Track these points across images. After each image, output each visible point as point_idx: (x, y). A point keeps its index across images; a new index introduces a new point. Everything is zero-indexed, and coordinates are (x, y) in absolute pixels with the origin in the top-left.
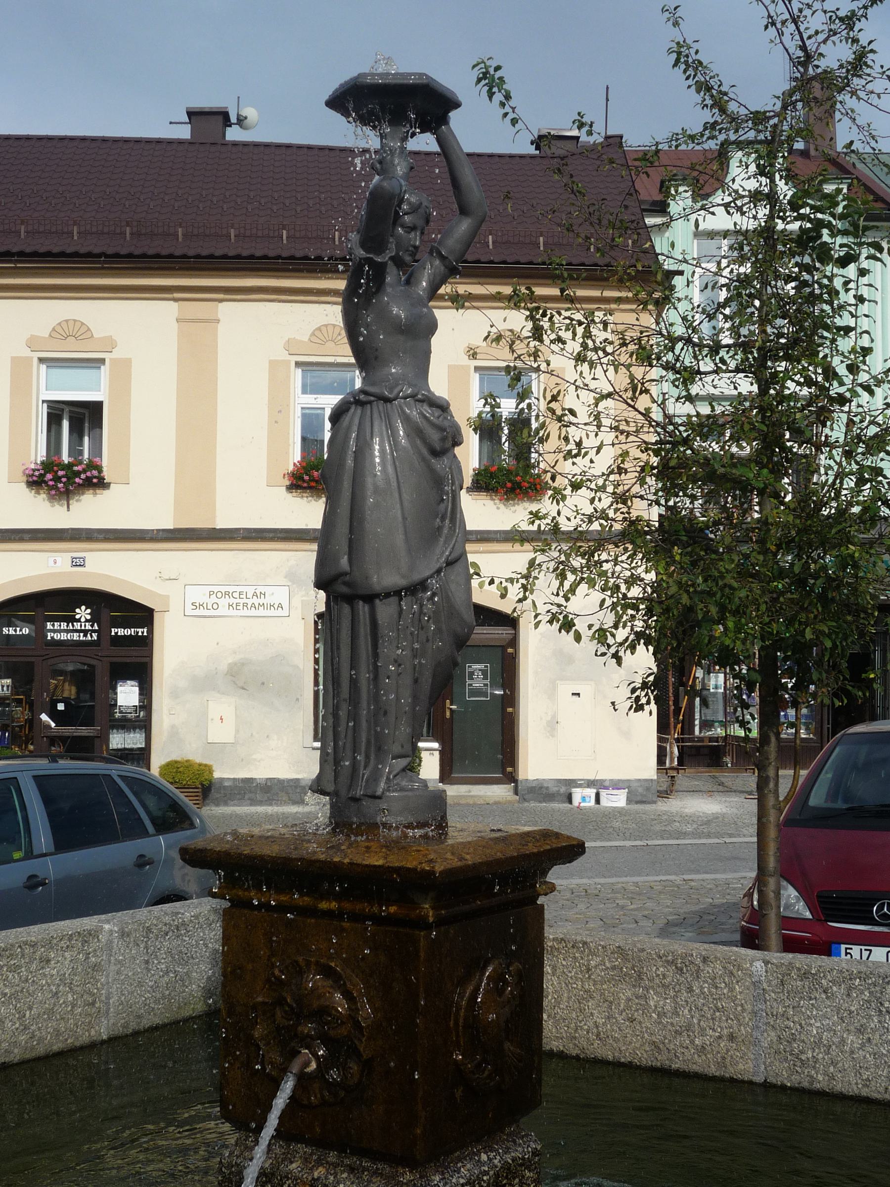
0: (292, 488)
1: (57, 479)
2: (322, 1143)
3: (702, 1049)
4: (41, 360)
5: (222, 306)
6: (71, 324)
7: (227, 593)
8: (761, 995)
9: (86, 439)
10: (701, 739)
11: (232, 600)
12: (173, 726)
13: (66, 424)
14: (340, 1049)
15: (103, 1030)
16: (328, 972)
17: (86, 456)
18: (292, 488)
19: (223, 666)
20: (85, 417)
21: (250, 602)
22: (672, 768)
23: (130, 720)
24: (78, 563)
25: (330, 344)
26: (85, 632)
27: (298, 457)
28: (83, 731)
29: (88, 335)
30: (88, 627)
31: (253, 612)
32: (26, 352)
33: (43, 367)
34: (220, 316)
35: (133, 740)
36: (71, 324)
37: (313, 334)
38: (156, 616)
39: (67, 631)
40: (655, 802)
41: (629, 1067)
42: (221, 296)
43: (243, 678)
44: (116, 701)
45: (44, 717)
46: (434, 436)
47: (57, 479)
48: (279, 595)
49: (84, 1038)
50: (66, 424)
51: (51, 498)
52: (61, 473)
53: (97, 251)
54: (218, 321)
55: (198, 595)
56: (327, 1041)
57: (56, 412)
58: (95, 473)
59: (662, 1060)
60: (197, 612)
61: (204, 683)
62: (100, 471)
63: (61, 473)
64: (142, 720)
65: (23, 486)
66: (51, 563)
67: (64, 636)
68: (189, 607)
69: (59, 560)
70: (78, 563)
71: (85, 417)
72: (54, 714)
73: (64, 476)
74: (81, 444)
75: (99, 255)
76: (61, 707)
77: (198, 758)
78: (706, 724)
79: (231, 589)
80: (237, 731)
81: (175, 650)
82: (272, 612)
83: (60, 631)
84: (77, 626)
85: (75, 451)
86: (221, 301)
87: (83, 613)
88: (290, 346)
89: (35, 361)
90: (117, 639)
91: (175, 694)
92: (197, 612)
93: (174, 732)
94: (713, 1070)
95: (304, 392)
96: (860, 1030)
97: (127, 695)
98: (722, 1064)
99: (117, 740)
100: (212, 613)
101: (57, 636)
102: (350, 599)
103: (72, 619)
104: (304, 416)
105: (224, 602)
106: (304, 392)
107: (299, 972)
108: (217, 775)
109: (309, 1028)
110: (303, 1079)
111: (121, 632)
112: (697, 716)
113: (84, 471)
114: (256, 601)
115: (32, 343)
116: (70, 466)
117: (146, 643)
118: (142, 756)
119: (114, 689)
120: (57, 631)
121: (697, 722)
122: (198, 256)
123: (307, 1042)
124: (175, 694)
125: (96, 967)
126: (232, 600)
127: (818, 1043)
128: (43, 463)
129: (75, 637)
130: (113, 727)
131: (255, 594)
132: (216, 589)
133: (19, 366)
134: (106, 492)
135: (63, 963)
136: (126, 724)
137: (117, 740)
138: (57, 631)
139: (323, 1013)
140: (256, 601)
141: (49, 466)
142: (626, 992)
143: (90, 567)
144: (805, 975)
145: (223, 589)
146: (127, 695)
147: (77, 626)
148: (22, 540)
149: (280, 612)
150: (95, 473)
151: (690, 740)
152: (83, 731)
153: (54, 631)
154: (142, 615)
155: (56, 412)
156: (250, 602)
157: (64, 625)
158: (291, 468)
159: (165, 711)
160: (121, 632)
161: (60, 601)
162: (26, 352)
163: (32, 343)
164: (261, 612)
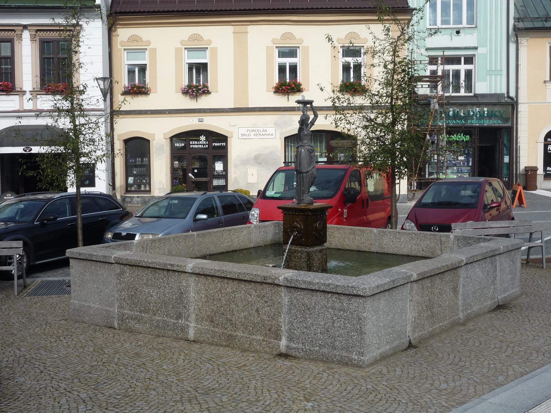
0: (276, 92)
1: (193, 91)
2: (297, 245)
3: (366, 247)
4: (185, 48)
5: (249, 27)
6: (196, 35)
7: (253, 130)
8: (376, 236)
9: (201, 75)
10: (428, 179)
11: (255, 133)
12: (235, 178)
13: (194, 71)
14: (299, 232)
15: (252, 245)
16: (297, 222)
17: (201, 83)
18: (276, 92)
19: (253, 156)
20: (201, 68)
21: (261, 133)
22: (414, 190)
23: (220, 175)
24: (201, 121)
25: (288, 40)
26: (204, 145)
27: (277, 81)
28: (204, 179)
29: (202, 39)
30: (205, 143)
31: (263, 137)
32: (180, 46)
33: (186, 51)
34: (248, 30)
35: (221, 182)
36: (196, 35)
37: (282, 36)
38: (229, 139)
39: (197, 144)
40: (406, 202)
41: (353, 251)
42: (249, 23)
43: (258, 160)
44: (215, 168)
45: (190, 175)
46: (311, 151)
47: (193, 91)
48: (271, 131)
49: (249, 247)
50: (194, 71)
51: (191, 98)
52: (194, 89)
53: (204, 9)
54: (248, 33)
55: (243, 131)
56: (297, 231)
57: (191, 67)
58: (206, 89)
59: (359, 249)
60: (243, 137)
61: (246, 162)
62: (208, 88)
63: (194, 89)
64: (224, 175)
65: (181, 94)
66: (191, 121)
67: (196, 146)
68: (240, 135)
69: (194, 120)
70: (201, 121)
71: (201, 68)
72: (194, 174)
73: (195, 90)
74: (200, 77)
75: (205, 11)
76: (196, 171)
77: (244, 189)
78: (430, 174)
79: (255, 129)
80: (258, 179)
81: (236, 150)
82: (269, 137)
83: (195, 144)
84: (201, 142)
85: (198, 81)
86: (249, 25)
87: (203, 138)
88: (273, 41)
89: (183, 49)
90: (215, 147)
91: (236, 166)
92: (243, 137)
93: (236, 179)
94: (368, 250)
95: (279, 57)
96: (393, 242)
97: (219, 166)
98: (369, 249)
99: (216, 182)
100: (248, 137)
101: (194, 146)
102: (300, 173)
103: (199, 140)
104: (279, 66)
105: (252, 133)
106: (279, 57)
107: (293, 222)
108: (251, 194)
109: (295, 229)
110: (294, 236)
111: (216, 144)
112: (427, 170)
113: (202, 88)
114: (264, 133)
115: (182, 42)
116: (197, 87)
117: (225, 148)
118: (225, 187)
119: (214, 164)
120: (194, 145)
121: (427, 173)
122: (240, 10)
123: (295, 231)
124: (236, 166)
125: (251, 233)
126: (255, 133)
127: (385, 244)
128: (188, 86)
129: (200, 146)
130: (214, 178)
131: (263, 131)
132: (249, 129)
133: (178, 52)
134: (210, 95)
135: (245, 232)
136: (218, 176)
137: (216, 182)
138: (194, 145)
139: (296, 227)
140: (264, 133)
141: (190, 86)
142: (352, 236)
143: (204, 123)
144: (383, 232)
145: (252, 129)
146: (219, 166)
147: (201, 142)
148: (181, 113)
149: (272, 137)
150: (206, 89)
151: (424, 180)
152: (204, 179)
153: (193, 144)
154: (224, 138)
155: (191, 67)
156: (261, 133)
157: (196, 142)
158: (275, 85)
159: (233, 172)
160: (216, 144)
161: (195, 134)
162: (180, 46)
163: (182, 42)
164: (265, 137)
